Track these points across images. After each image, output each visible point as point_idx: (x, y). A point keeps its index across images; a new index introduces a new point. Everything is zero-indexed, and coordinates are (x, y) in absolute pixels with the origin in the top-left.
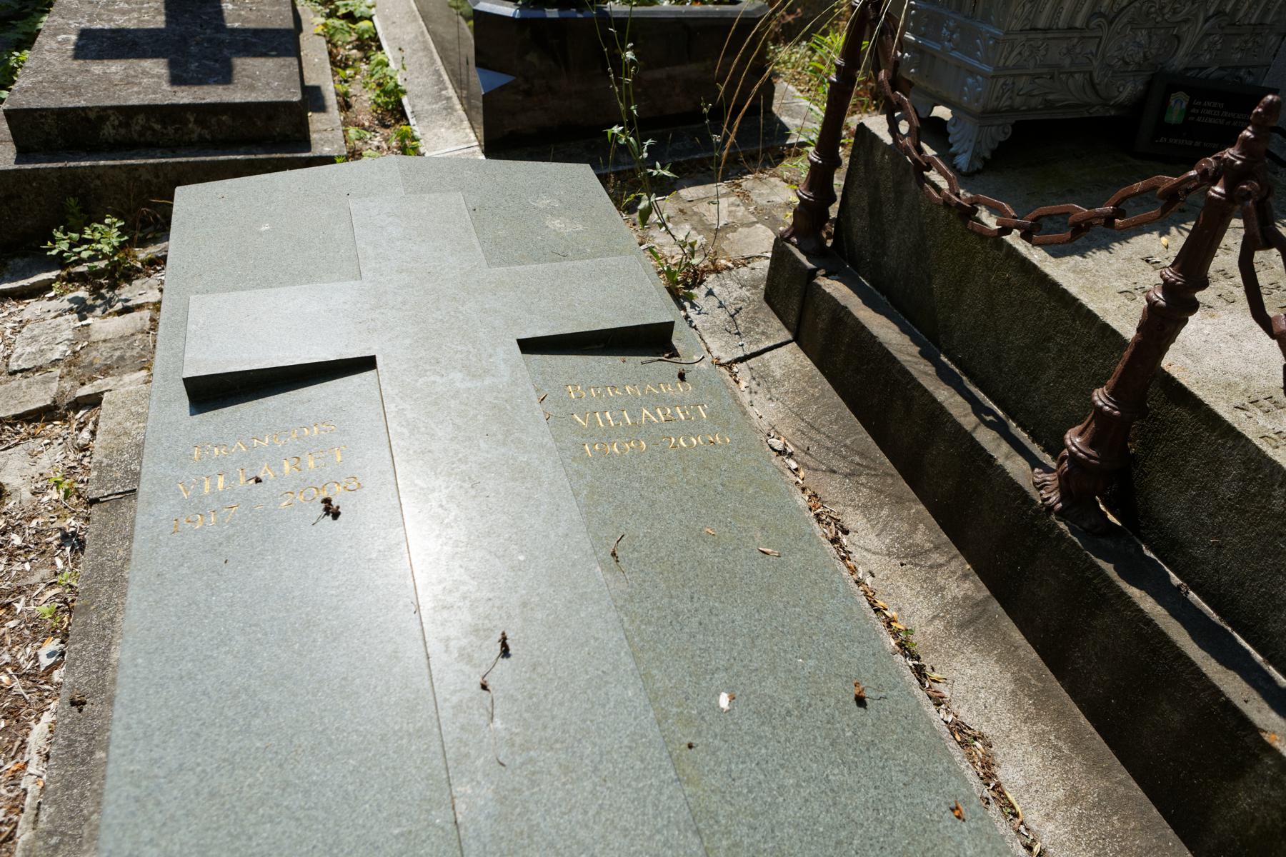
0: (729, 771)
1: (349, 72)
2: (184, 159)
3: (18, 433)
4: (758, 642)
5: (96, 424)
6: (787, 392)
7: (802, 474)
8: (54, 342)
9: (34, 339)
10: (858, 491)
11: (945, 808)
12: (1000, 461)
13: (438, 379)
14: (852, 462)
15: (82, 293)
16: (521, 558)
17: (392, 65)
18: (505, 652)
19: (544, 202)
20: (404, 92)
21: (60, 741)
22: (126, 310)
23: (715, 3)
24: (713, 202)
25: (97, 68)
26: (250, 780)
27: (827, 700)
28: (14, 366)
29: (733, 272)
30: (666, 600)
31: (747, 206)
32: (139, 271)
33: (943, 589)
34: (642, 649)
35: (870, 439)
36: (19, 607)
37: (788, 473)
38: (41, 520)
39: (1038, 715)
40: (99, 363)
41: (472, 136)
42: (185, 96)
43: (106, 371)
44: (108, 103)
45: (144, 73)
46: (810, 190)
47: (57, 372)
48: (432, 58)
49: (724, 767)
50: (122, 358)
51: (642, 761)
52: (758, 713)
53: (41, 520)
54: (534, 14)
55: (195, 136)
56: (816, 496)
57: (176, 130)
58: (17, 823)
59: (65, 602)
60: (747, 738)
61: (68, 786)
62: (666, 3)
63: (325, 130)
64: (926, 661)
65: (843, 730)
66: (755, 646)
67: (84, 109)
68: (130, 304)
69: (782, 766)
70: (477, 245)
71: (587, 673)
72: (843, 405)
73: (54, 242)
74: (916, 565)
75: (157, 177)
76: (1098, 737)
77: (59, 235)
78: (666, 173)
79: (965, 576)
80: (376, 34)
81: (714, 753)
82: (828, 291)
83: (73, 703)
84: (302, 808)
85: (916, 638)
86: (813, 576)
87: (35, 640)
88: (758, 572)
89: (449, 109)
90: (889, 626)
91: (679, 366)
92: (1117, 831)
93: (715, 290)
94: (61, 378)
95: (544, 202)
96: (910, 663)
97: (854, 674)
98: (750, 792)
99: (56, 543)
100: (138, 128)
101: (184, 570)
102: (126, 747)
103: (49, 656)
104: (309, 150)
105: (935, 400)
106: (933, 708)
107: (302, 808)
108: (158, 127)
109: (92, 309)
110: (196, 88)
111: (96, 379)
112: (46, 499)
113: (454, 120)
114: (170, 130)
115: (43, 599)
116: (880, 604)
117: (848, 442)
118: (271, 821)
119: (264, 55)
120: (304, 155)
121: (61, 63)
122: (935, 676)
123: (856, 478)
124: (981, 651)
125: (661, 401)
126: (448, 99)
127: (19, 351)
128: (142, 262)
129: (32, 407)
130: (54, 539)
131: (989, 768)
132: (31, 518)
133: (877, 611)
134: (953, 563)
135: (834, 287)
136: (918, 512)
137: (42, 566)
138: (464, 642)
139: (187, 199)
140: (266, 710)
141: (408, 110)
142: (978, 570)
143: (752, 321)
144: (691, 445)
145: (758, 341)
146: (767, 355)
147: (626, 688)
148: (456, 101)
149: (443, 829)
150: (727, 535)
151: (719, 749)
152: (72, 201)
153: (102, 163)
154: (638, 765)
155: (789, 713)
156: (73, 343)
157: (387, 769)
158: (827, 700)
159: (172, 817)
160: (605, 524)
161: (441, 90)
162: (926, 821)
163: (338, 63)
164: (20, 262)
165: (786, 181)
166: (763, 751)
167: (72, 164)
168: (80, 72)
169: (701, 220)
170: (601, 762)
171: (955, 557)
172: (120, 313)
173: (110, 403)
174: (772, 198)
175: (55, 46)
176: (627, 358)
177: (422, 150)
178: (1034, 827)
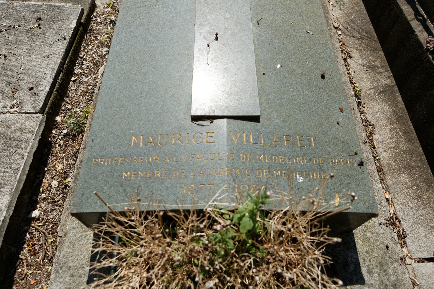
0: (273, 83)
6: (347, 8)
7: (341, 36)
10: (360, 45)
11: (338, 108)
12: (416, 33)
14: (362, 35)
16: (228, 16)
27: (312, 74)
33: (379, 80)
34: (258, 48)
35: (372, 28)
36: (99, 38)
37: (337, 35)
38: (105, 16)
39: (396, 123)
49: (272, 81)
53: (105, 16)
56: (344, 44)
64: (363, 101)
69: (290, 86)
72: (367, 14)
76: (415, 133)
79: (389, 77)
85: (362, 95)
87: (102, 47)
90: (354, 88)
92: (408, 159)
96: (357, 100)
98: (278, 89)
101: (134, 6)
103: (105, 51)
105: (401, 9)
106: (359, 114)
112: (107, 10)
116: (354, 81)
117: (363, 28)
122: (364, 106)
124: (384, 101)
130: (108, 21)
131: (371, 134)
132: (103, 15)
133: (352, 83)
134: (386, 73)
136: (380, 55)
138: (206, 34)
140: (150, 43)
142: (394, 76)
160: (258, 14)
162: (330, 109)
171: (388, 71)
178: (379, 153)
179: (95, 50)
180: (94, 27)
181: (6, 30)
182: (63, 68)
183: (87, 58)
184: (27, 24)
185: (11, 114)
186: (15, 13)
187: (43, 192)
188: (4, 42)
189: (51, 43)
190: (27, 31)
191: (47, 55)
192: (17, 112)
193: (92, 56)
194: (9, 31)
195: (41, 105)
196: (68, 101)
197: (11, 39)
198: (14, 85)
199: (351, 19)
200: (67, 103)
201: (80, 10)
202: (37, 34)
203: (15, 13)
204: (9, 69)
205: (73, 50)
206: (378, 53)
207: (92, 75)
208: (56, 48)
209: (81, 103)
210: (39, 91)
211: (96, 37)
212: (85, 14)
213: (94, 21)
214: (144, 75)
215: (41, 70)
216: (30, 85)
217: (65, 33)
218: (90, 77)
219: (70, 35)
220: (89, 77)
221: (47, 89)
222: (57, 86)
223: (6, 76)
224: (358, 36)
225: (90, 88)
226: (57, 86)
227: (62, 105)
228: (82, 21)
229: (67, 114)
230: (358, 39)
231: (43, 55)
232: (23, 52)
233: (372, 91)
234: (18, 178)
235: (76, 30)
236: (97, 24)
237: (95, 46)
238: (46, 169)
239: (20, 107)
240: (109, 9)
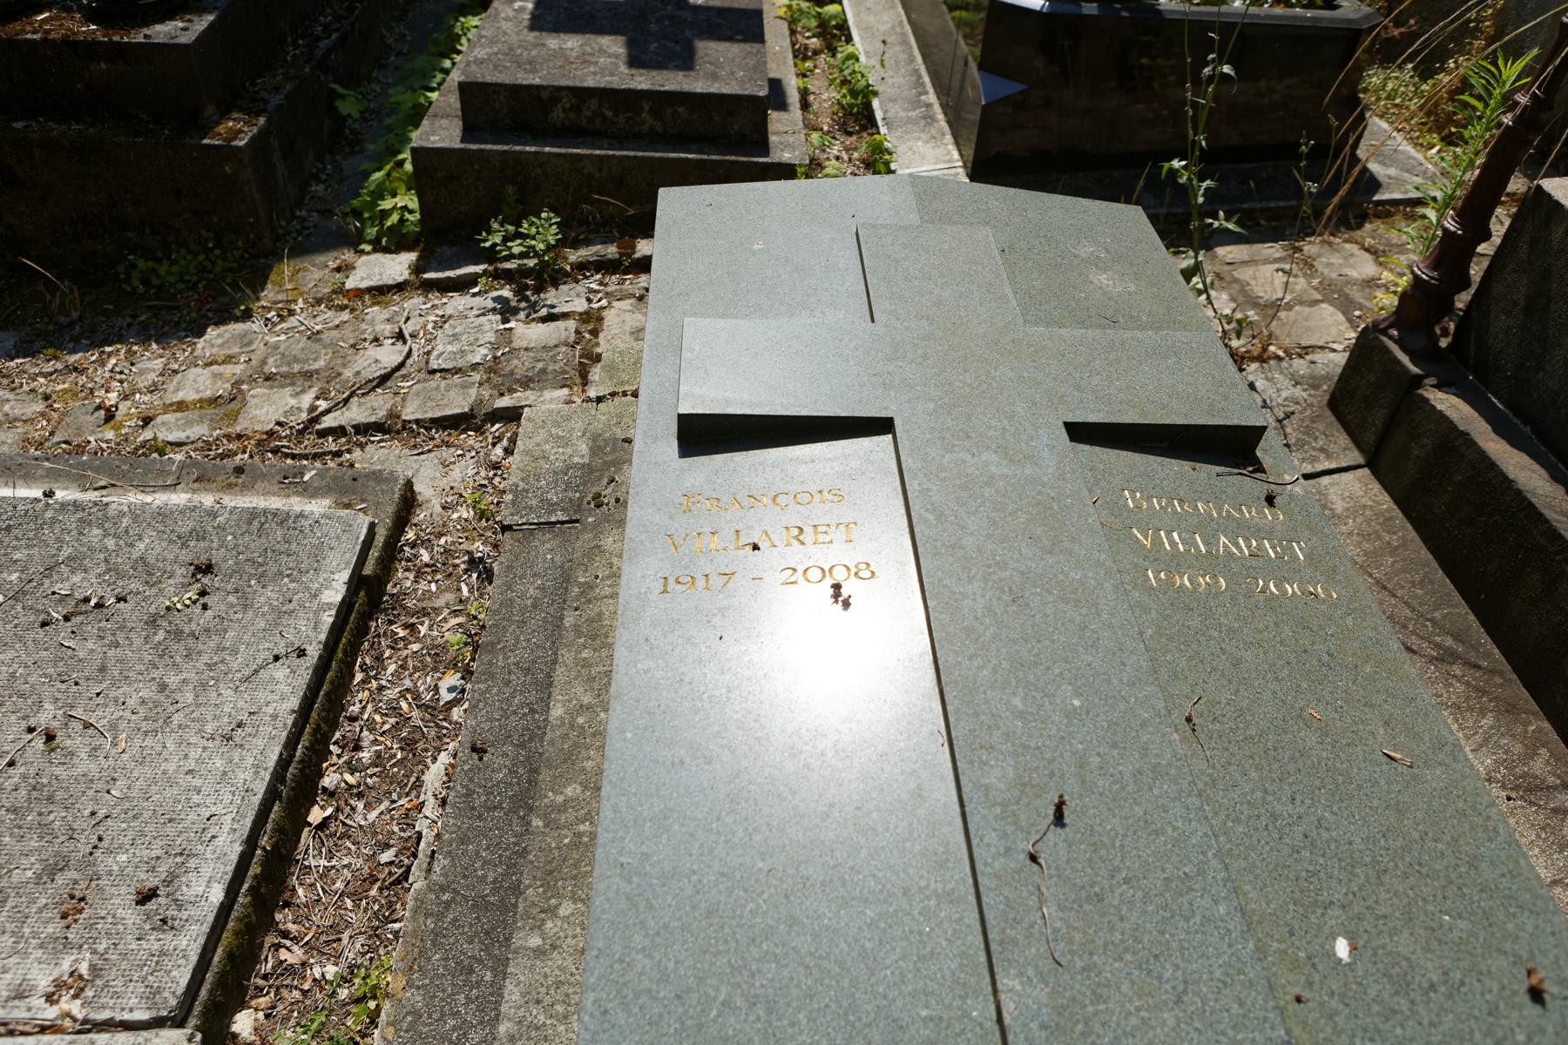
1: (809, 64)
2: (632, 153)
3: (433, 439)
4: (1386, 879)
5: (513, 441)
8: (475, 343)
10: (1448, 685)
13: (967, 457)
15: (506, 293)
16: (1076, 703)
17: (862, 59)
18: (1059, 819)
19: (1086, 250)
20: (876, 94)
21: (459, 788)
22: (551, 318)
23: (1304, 7)
24: (1261, 269)
25: (553, 42)
26: (752, 906)
27: (1488, 982)
28: (434, 365)
29: (1284, 364)
30: (1259, 794)
31: (1309, 277)
32: (567, 275)
35: (1472, 617)
36: (423, 630)
38: (450, 539)
40: (519, 373)
41: (956, 155)
42: (643, 81)
43: (526, 383)
44: (563, 82)
45: (602, 51)
46: (1435, 269)
47: (476, 377)
48: (911, 55)
50: (544, 371)
51: (1241, 1005)
52: (1390, 977)
54: (1069, 9)
55: (645, 128)
57: (628, 119)
58: (409, 868)
59: (470, 636)
60: (1376, 1008)
61: (464, 841)
62: (1237, 4)
63: (787, 136)
65: (1512, 1030)
66: (1382, 884)
67: (538, 87)
68: (555, 311)
70: (1011, 296)
71: (1163, 870)
72: (1434, 564)
73: (489, 232)
74: (1531, 803)
75: (601, 170)
77: (496, 226)
78: (1231, 226)
80: (845, 21)
81: (1331, 1017)
82: (1439, 407)
83: (474, 749)
84: (811, 954)
86: (1460, 804)
87: (435, 669)
88: (1383, 782)
89: (929, 119)
91: (1266, 486)
93: (1257, 384)
94: (481, 384)
95: (1086, 250)
97: (1525, 955)
99: (463, 566)
100: (589, 113)
102: (616, 832)
103: (450, 690)
104: (767, 155)
107: (811, 954)
108: (609, 114)
109: (515, 311)
110: (654, 73)
111: (516, 391)
112: (455, 516)
113: (934, 132)
114: (622, 118)
115: (447, 626)
117: (1437, 614)
118: (777, 961)
120: (761, 160)
121: (517, 34)
123: (1445, 667)
125: (1239, 528)
126: (929, 106)
127: (440, 348)
128: (572, 265)
129: (449, 412)
130: (461, 562)
132: (440, 535)
135: (1446, 403)
136: (1539, 730)
137: (448, 589)
139: (672, 202)
141: (879, 115)
143: (1308, 431)
144: (1285, 593)
145: (1314, 460)
146: (1325, 480)
147: (1216, 902)
148: (937, 109)
149: (981, 1025)
150: (1338, 724)
151: (1338, 1013)
152: (510, 189)
153: (547, 149)
154: (1235, 1009)
155: (1432, 986)
157: (911, 932)
158: (1488, 982)
159: (666, 926)
161: (921, 94)
163: (801, 54)
164: (447, 251)
165: (1367, 250)
166: (1399, 1031)
167: (518, 148)
168: (535, 46)
169: (1243, 290)
170: (1185, 991)
172: (544, 320)
173: (529, 420)
174: (1346, 271)
175: (511, 14)
176: (1198, 465)
177: (893, 166)
179: (408, 683)
180: (408, 583)
181: (67, 619)
182: (283, 782)
183: (378, 718)
184: (154, 591)
185: (43, 1030)
186: (110, 543)
188: (51, 671)
189: (247, 672)
190: (152, 622)
191: (225, 724)
192: (75, 1020)
193: (395, 710)
194: (79, 619)
195: (183, 977)
196: (292, 927)
197: (81, 655)
198: (75, 875)
199: (1378, 582)
200: (286, 934)
201: (364, 531)
202: (192, 634)
203: (110, 543)
204: (60, 795)
205: (327, 694)
206: (1530, 723)
207: (395, 796)
208: (262, 696)
209: (345, 936)
210: (180, 908)
211: (411, 627)
212: (380, 539)
213: (409, 560)
214: (769, 1011)
215: (196, 799)
216: (143, 876)
217: (302, 624)
218: (386, 803)
219: (323, 637)
220: (382, 807)
221: (217, 895)
222: (255, 869)
223: (45, 830)
225: (386, 857)
226: (255, 869)
227: (261, 946)
228: (368, 570)
229: (285, 992)
230: (1432, 660)
231: (209, 729)
232: (127, 714)
235: (345, 608)
236: (419, 575)
237: (410, 663)
239: (89, 993)
240: (465, 513)
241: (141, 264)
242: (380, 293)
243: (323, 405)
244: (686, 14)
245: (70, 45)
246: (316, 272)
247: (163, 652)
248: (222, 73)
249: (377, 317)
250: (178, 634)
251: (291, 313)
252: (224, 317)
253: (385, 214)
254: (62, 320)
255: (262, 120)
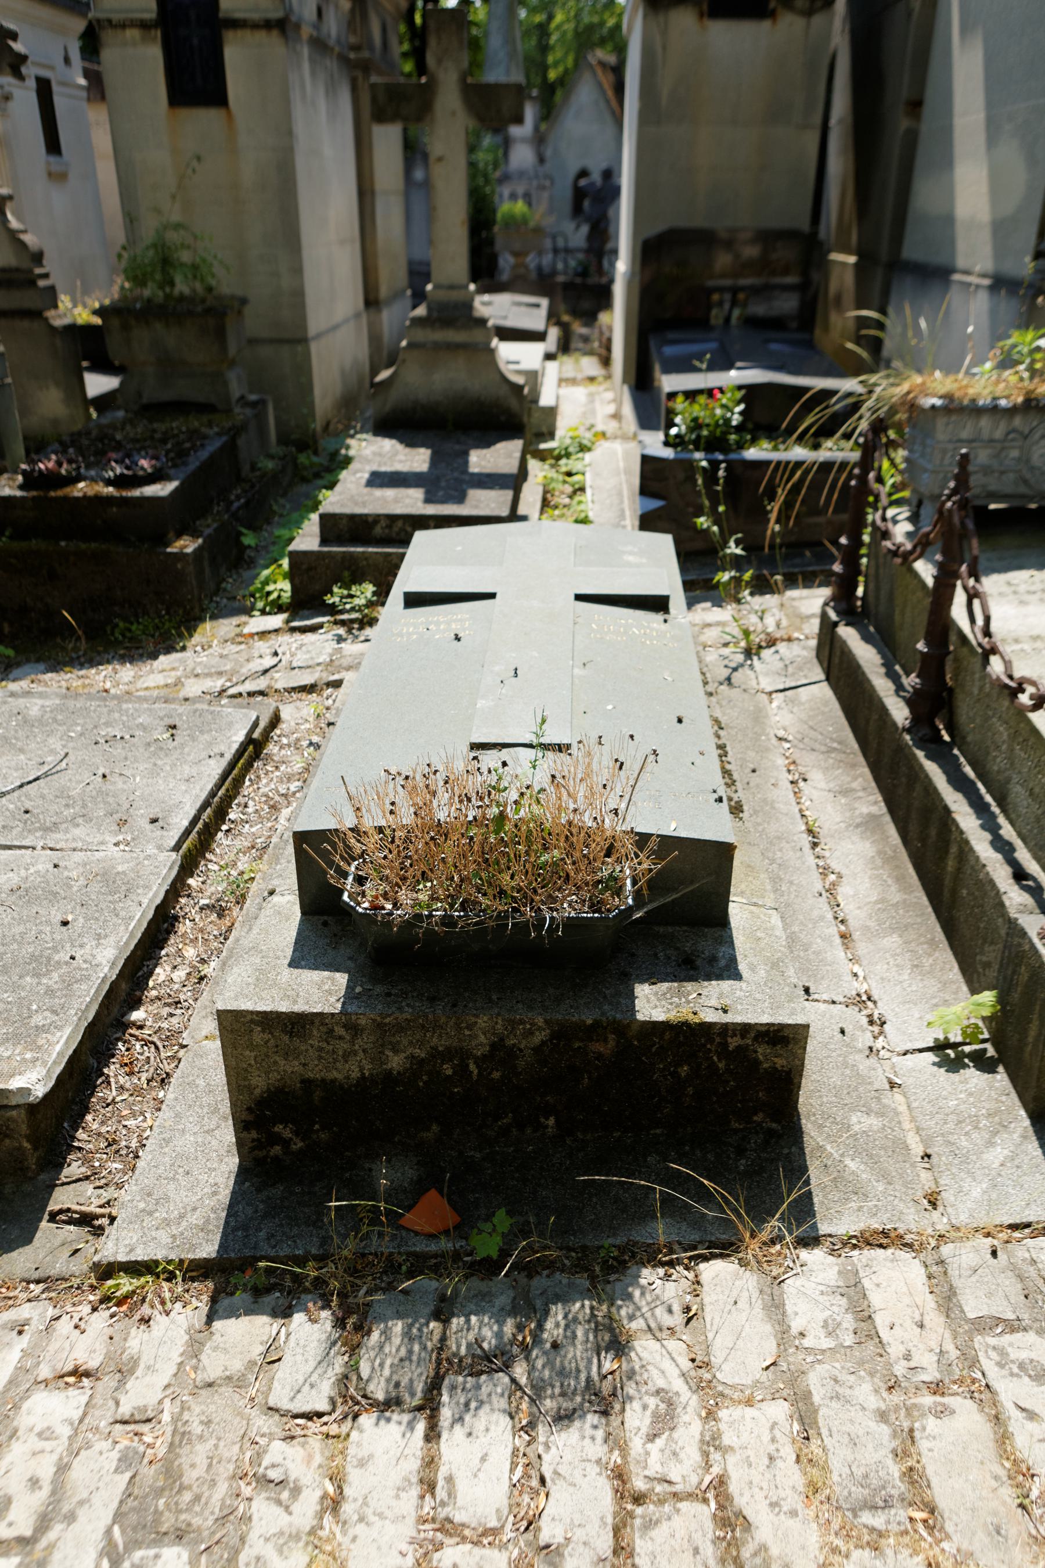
9: (308, 652)
10: (826, 761)
18: (516, 675)
28: (294, 664)
43: (348, 668)
45: (408, 496)
47: (319, 668)
67: (366, 515)
79: (876, 803)
109: (345, 640)
119: (491, 488)
130: (305, 743)
156: (331, 655)
164: (306, 612)
186: (125, 718)
187: (154, 988)
190: (149, 744)
221: (186, 823)
224: (823, 749)
226: (200, 825)
233: (843, 825)
234: (131, 928)
238: (163, 953)
241: (121, 625)
242: (263, 634)
243: (228, 684)
244: (467, 478)
245: (98, 499)
246: (226, 626)
247: (154, 754)
248: (180, 513)
249: (262, 647)
250: (161, 749)
251: (210, 646)
252: (169, 650)
253: (269, 593)
254: (74, 655)
255: (200, 541)
